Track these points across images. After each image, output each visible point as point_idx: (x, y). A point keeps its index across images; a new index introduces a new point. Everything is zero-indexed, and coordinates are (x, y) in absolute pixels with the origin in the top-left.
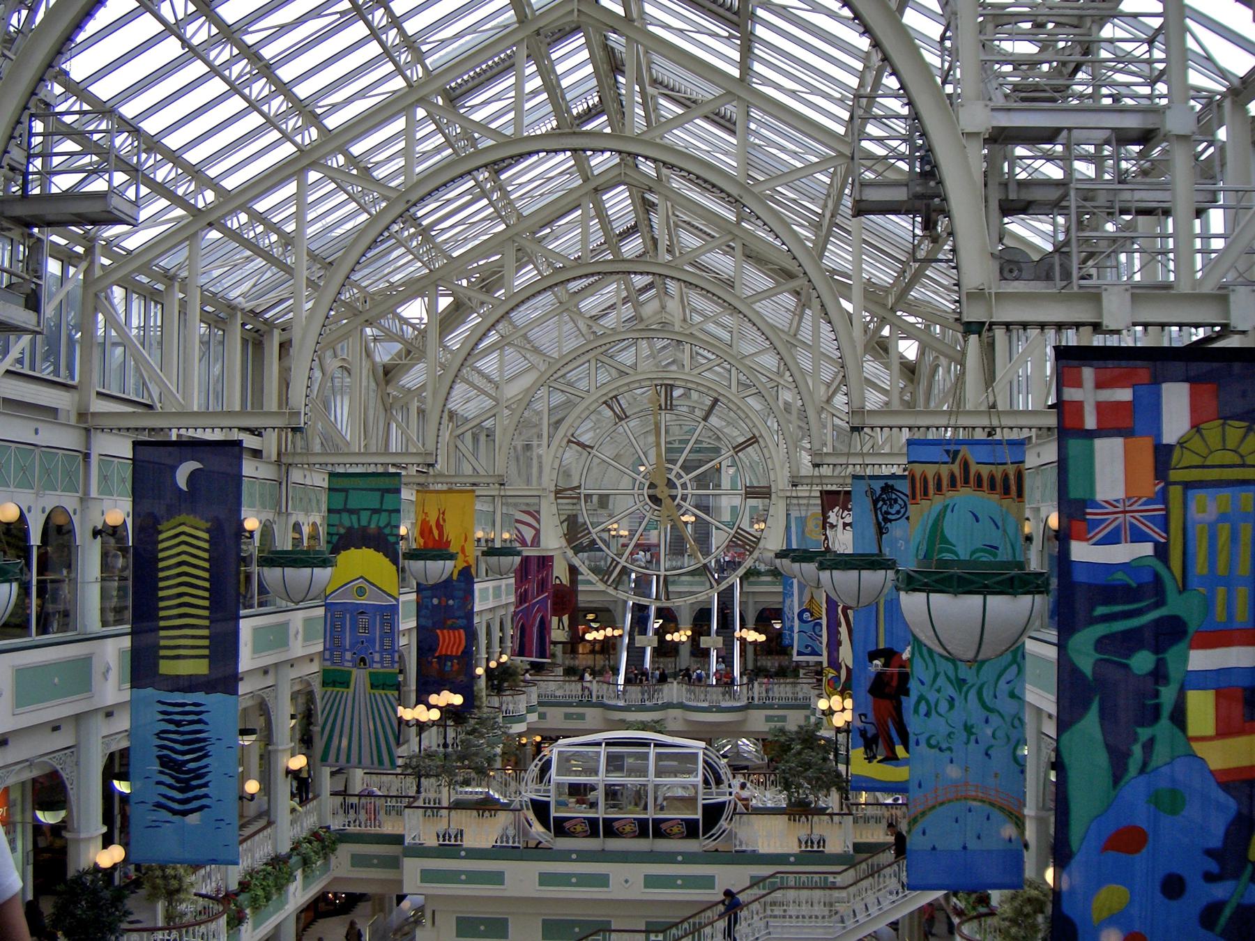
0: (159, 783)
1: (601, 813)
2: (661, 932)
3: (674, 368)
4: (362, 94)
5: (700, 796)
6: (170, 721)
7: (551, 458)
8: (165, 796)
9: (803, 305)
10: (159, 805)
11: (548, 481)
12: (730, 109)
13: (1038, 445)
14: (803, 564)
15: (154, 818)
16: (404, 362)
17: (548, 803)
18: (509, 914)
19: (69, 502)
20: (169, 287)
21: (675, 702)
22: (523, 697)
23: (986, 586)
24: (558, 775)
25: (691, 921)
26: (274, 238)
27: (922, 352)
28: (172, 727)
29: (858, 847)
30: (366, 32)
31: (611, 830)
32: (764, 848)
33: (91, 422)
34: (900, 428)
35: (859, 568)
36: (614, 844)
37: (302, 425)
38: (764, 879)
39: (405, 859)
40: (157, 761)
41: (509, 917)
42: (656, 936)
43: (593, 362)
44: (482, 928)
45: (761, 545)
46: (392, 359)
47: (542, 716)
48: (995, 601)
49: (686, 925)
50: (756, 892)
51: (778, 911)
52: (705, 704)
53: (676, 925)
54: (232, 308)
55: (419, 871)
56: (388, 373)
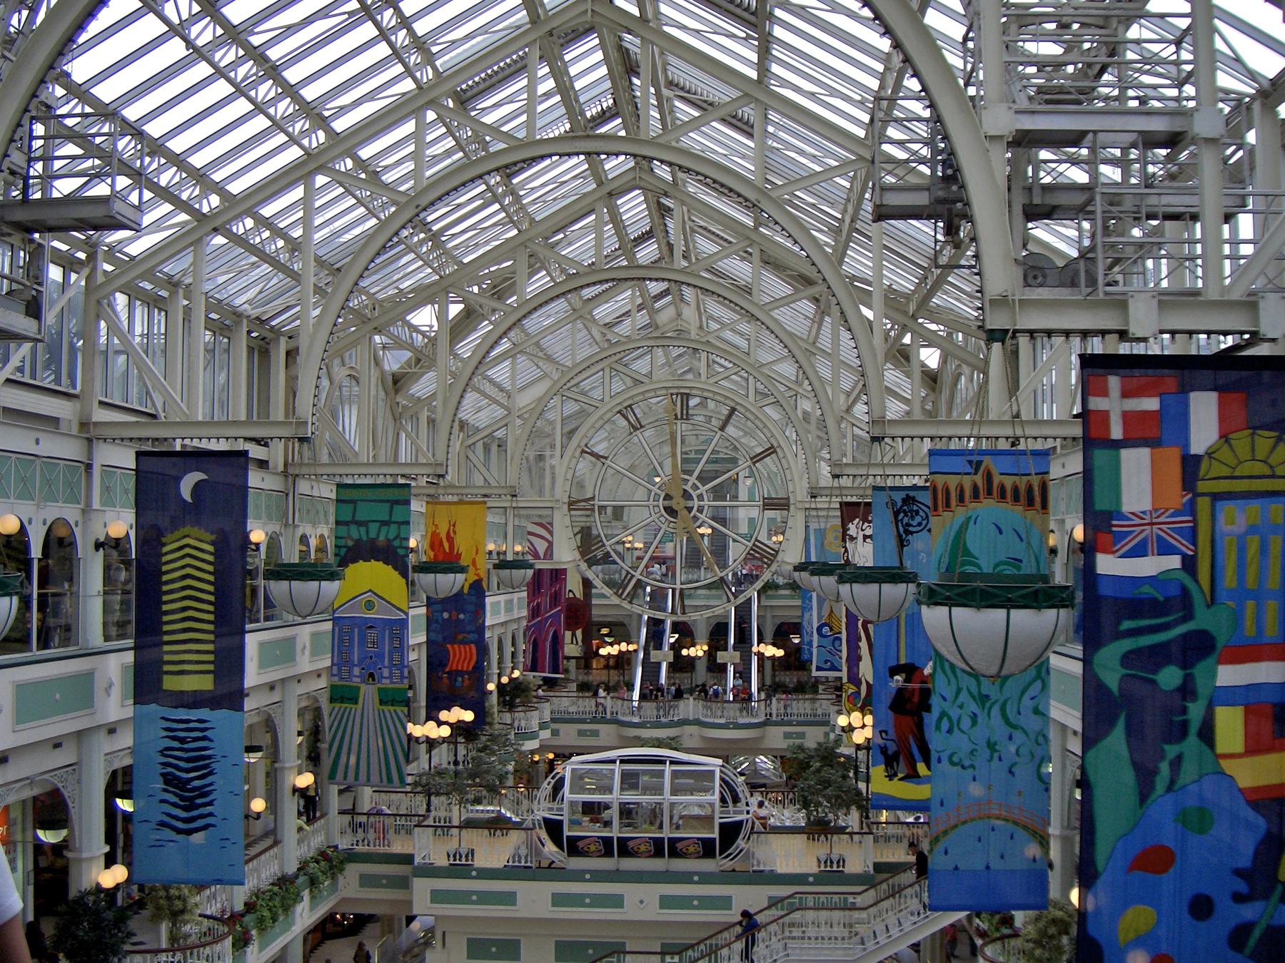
0: (163, 801)
1: (615, 832)
2: (677, 954)
3: (690, 376)
4: (370, 96)
5: (717, 815)
6: (174, 738)
7: (564, 469)
8: (169, 815)
9: (822, 313)
10: (163, 824)
11: (562, 492)
12: (748, 112)
13: (1062, 455)
14: (822, 577)
15: (158, 837)
16: (413, 370)
17: (561, 822)
18: (521, 935)
19: (71, 513)
20: (173, 294)
21: (691, 718)
22: (536, 713)
23: (1010, 600)
24: (571, 793)
25: (708, 942)
26: (281, 243)
27: (944, 360)
28: (176, 744)
29: (879, 867)
30: (375, 32)
31: (626, 849)
32: (782, 868)
33: (93, 432)
34: (922, 438)
35: (880, 581)
36: (629, 864)
37: (309, 435)
38: (782, 899)
39: (415, 879)
40: (161, 779)
41: (522, 939)
42: (672, 958)
43: (607, 371)
44: (494, 949)
45: (779, 558)
46: (402, 367)
47: (555, 733)
48: (1019, 615)
49: (702, 947)
50: (775, 912)
51: (796, 932)
52: (722, 721)
53: (692, 946)
54: (237, 315)
55: (429, 892)
56: (398, 382)
